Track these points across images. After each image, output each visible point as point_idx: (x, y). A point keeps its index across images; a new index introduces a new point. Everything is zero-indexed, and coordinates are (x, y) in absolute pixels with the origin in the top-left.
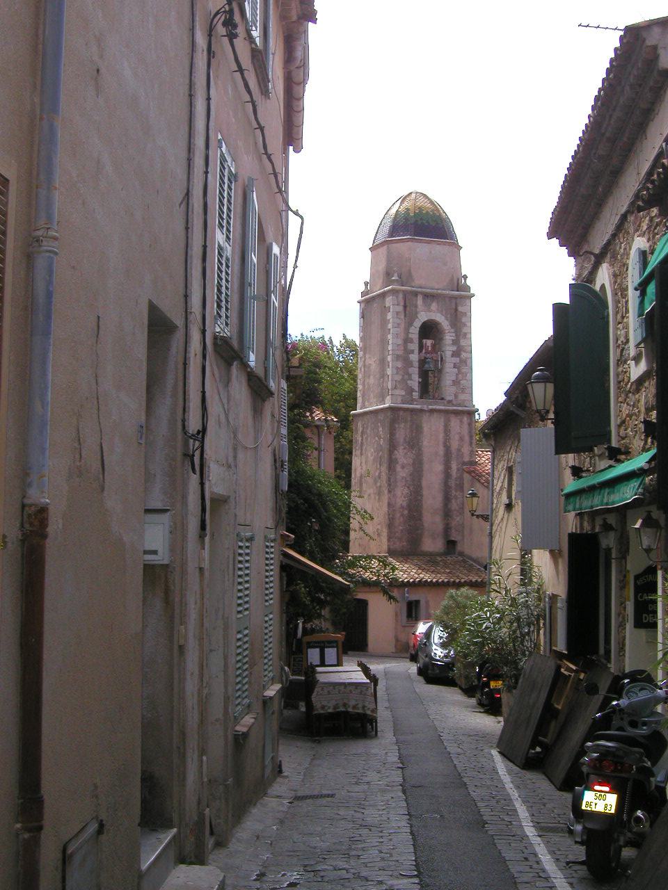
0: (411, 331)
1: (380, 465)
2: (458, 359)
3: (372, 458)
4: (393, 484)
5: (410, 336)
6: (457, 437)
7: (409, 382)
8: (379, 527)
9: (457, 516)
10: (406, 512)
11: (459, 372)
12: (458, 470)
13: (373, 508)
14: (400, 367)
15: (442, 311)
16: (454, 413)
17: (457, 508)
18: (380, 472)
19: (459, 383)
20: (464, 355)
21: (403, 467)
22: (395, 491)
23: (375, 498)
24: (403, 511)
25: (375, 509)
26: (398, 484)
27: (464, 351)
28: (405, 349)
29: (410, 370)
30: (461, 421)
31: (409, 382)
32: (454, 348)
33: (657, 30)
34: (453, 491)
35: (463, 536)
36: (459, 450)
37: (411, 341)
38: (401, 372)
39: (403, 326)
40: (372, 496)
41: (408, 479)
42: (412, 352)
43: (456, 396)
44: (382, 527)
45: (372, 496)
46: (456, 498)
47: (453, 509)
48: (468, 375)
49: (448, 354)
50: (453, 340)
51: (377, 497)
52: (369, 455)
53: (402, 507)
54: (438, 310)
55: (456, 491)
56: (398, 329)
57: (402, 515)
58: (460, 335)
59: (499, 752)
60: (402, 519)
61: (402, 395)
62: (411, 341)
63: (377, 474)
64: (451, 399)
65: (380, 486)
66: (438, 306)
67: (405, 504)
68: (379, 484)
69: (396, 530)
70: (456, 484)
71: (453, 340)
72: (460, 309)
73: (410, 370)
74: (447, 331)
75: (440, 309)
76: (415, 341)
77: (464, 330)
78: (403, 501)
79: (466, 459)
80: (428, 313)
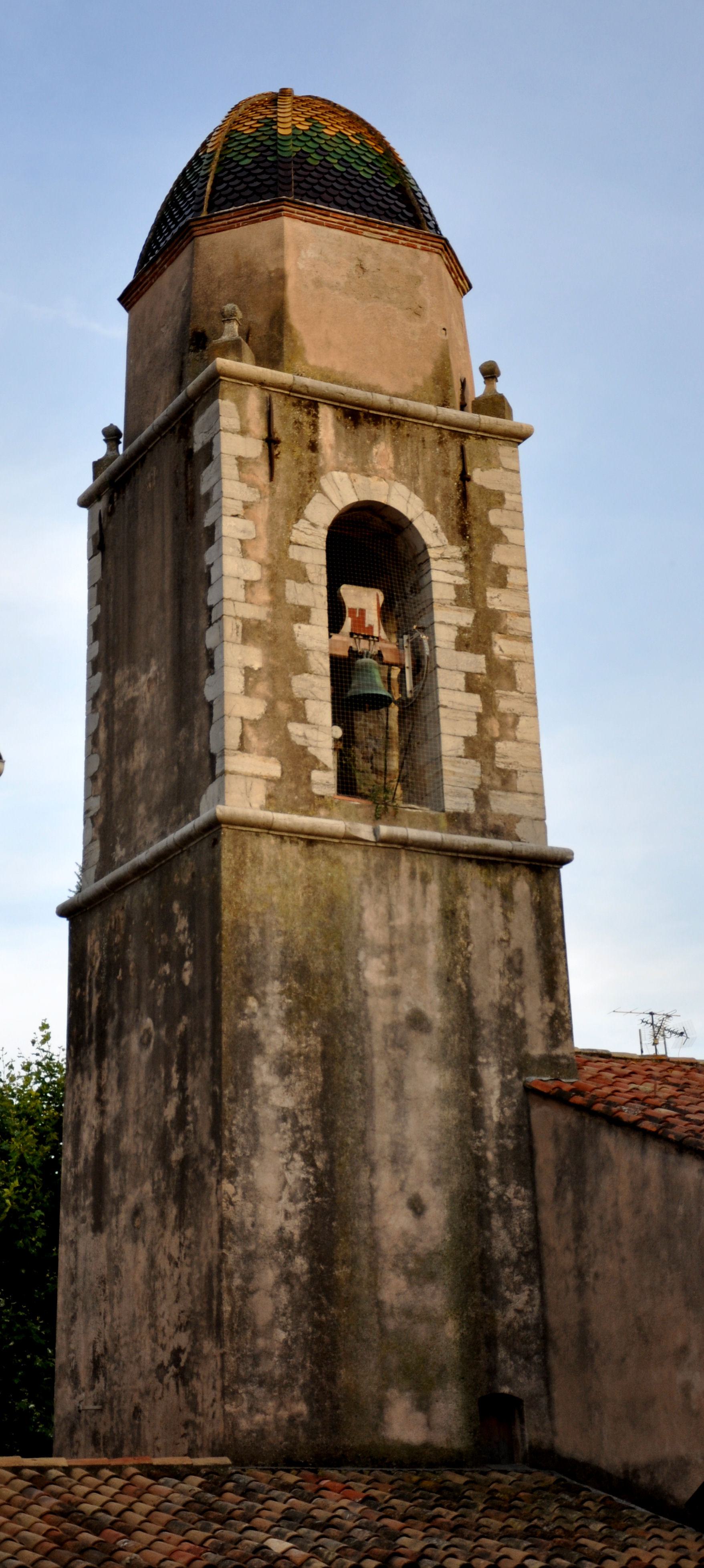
0: (295, 536)
1: (183, 1071)
2: (482, 658)
3: (146, 1055)
4: (241, 1139)
5: (294, 553)
6: (497, 958)
7: (296, 729)
8: (183, 1340)
9: (517, 1290)
10: (300, 1264)
11: (489, 704)
12: (506, 1089)
13: (152, 1262)
14: (257, 665)
15: (414, 478)
16: (480, 863)
17: (514, 1255)
18: (185, 1101)
19: (491, 749)
20: (503, 647)
21: (283, 1070)
22: (249, 1169)
23: (163, 1215)
24: (290, 1258)
25: (163, 1263)
26: (265, 1140)
27: (503, 632)
28: (277, 599)
29: (300, 684)
30: (507, 896)
31: (296, 729)
32: (466, 618)
33: (559, 915)
34: (493, 1181)
35: (547, 1379)
36: (505, 1012)
37: (301, 575)
38: (262, 687)
39: (262, 512)
40: (151, 1211)
41: (304, 1121)
42: (303, 615)
43: (481, 798)
44: (195, 1339)
45: (151, 1211)
46: (506, 1210)
47: (497, 1255)
48: (522, 722)
49: (445, 636)
50: (458, 588)
51: (172, 1212)
52: (135, 1047)
53: (284, 1242)
54: (395, 469)
55: (504, 1182)
56: (248, 524)
57: (287, 1278)
58: (483, 573)
59: (166, 1107)
60: (284, 1296)
61: (269, 780)
62: (301, 575)
63: (170, 1112)
64: (462, 809)
65: (184, 1163)
66: (397, 456)
67: (294, 1227)
68: (177, 1154)
69: (261, 1343)
70: (502, 1152)
71: (458, 588)
72: (479, 476)
73: (300, 684)
74: (432, 553)
75: (406, 470)
76: (312, 576)
77: (500, 555)
78: (287, 1215)
79: (537, 1048)
80: (360, 479)
